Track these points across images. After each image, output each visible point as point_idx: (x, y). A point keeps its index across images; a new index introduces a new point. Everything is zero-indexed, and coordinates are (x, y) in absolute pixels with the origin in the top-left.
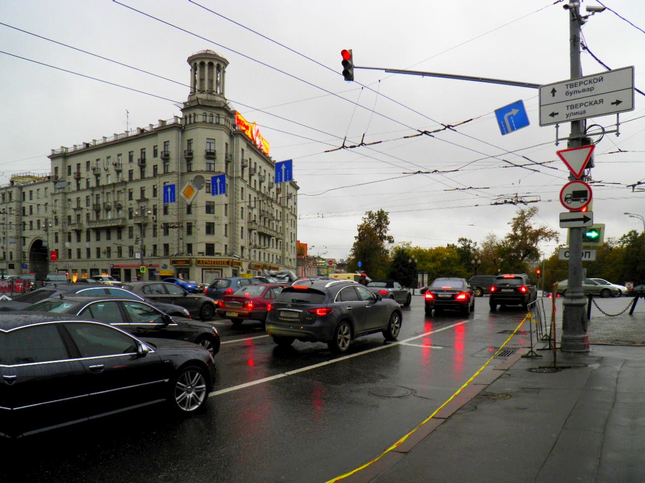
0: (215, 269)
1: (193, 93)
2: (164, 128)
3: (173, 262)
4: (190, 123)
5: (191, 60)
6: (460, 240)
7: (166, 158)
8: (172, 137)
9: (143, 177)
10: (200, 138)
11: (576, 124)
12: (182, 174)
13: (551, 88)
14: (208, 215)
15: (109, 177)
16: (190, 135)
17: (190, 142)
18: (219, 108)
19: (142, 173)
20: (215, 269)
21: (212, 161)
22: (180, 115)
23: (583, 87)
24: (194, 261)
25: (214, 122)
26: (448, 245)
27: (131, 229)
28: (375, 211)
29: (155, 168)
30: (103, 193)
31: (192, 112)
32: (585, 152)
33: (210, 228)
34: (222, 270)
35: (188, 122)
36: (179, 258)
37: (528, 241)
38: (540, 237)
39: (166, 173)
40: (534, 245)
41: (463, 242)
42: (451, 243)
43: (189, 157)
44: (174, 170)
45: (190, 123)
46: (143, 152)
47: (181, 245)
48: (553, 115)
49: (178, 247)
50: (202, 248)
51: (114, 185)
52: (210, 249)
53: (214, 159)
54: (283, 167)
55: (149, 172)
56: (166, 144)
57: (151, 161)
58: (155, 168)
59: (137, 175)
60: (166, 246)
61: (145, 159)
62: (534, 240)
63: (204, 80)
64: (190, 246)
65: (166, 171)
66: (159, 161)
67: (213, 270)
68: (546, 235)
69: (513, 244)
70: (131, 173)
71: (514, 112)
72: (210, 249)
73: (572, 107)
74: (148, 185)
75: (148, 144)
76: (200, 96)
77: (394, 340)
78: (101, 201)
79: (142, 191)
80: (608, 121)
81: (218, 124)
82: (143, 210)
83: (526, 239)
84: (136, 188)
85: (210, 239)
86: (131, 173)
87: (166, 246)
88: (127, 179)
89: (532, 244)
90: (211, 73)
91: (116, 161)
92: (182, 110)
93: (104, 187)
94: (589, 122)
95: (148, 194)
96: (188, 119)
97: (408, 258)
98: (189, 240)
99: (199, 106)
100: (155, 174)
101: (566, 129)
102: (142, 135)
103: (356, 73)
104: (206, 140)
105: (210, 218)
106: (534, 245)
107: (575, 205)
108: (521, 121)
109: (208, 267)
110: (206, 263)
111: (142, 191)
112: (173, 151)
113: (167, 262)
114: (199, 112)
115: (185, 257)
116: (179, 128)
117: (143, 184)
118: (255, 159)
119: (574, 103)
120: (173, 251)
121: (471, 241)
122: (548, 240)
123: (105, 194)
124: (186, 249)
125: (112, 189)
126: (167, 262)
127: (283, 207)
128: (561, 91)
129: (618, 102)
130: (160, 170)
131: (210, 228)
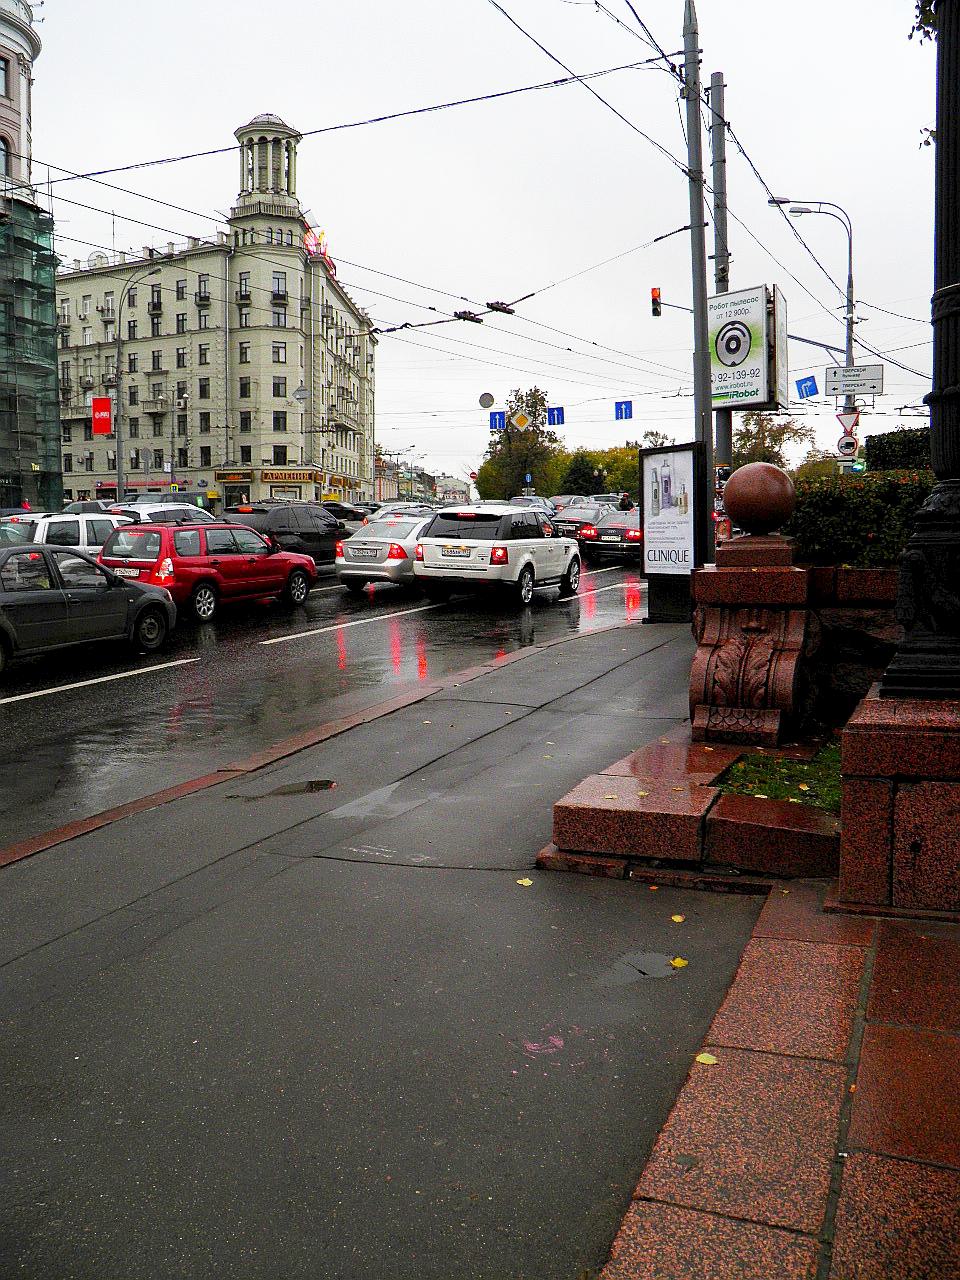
0: (289, 487)
1: (245, 193)
2: (200, 251)
3: (219, 477)
4: (245, 244)
5: (240, 134)
6: (646, 436)
7: (203, 302)
8: (215, 266)
9: (156, 334)
10: (262, 273)
11: (848, 397)
12: (231, 331)
13: (833, 371)
14: (276, 399)
15: (88, 331)
16: (244, 263)
17: (244, 277)
18: (287, 219)
19: (155, 326)
20: (289, 487)
21: (282, 310)
22: (227, 229)
23: (853, 373)
24: (258, 474)
25: (275, 242)
26: (628, 443)
27: (134, 422)
28: (524, 391)
29: (181, 320)
30: (77, 359)
31: (247, 226)
32: (854, 416)
33: (280, 422)
34: (300, 487)
35: (241, 243)
36: (230, 470)
37: (768, 443)
38: (786, 436)
39: (203, 329)
40: (776, 449)
41: (652, 438)
42: (632, 441)
43: (244, 300)
44: (219, 324)
45: (245, 244)
46: (156, 290)
47: (231, 450)
48: (834, 389)
49: (227, 453)
50: (269, 454)
51: (99, 345)
52: (280, 454)
53: (284, 306)
54: (623, 407)
55: (168, 325)
56: (203, 278)
57: (171, 306)
58: (181, 320)
59: (144, 330)
60: (206, 452)
61: (160, 303)
62: (775, 441)
63: (266, 168)
64: (246, 452)
65: (203, 326)
66: (189, 306)
67: (287, 489)
68: (796, 432)
69: (742, 447)
70: (132, 327)
71: (809, 383)
72: (280, 454)
73: (847, 385)
74: (168, 350)
75: (168, 278)
76: (261, 198)
77: (573, 592)
78: (73, 373)
79: (156, 358)
80: (868, 399)
81: (290, 245)
82: (157, 389)
83: (764, 438)
84: (144, 353)
85: (280, 439)
86: (132, 327)
87: (206, 452)
88: (125, 336)
89: (773, 447)
90: (277, 157)
91: (102, 304)
92: (230, 222)
93: (78, 348)
94: (857, 397)
95: (168, 363)
96: (240, 237)
97: (592, 469)
98: (246, 440)
99: (260, 216)
100: (181, 330)
101: (842, 400)
102: (154, 261)
103: (663, 309)
104: (272, 275)
105: (279, 404)
106: (776, 449)
107: (848, 451)
108: (814, 391)
109: (279, 484)
110: (276, 478)
111: (156, 358)
112: (215, 289)
113: (209, 476)
114: (261, 225)
115: (241, 468)
116: (228, 252)
117: (156, 345)
118: (334, 301)
119: (847, 383)
120: (218, 458)
121: (665, 437)
122: (799, 442)
123: (81, 362)
124: (239, 455)
125: (97, 352)
126: (209, 476)
127: (361, 379)
128: (840, 372)
129: (874, 387)
130: (192, 324)
131: (280, 422)
